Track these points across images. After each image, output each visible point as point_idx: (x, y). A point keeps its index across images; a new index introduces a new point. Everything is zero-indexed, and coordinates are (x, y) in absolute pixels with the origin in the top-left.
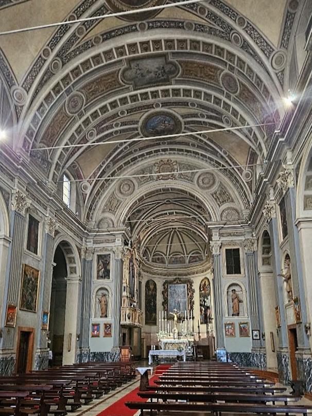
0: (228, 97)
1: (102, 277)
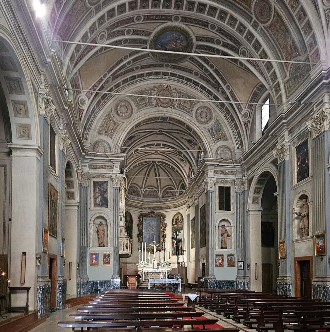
0: (255, 26)
1: (99, 205)
